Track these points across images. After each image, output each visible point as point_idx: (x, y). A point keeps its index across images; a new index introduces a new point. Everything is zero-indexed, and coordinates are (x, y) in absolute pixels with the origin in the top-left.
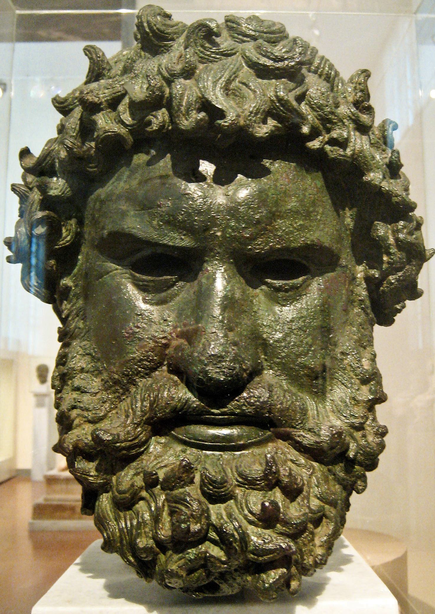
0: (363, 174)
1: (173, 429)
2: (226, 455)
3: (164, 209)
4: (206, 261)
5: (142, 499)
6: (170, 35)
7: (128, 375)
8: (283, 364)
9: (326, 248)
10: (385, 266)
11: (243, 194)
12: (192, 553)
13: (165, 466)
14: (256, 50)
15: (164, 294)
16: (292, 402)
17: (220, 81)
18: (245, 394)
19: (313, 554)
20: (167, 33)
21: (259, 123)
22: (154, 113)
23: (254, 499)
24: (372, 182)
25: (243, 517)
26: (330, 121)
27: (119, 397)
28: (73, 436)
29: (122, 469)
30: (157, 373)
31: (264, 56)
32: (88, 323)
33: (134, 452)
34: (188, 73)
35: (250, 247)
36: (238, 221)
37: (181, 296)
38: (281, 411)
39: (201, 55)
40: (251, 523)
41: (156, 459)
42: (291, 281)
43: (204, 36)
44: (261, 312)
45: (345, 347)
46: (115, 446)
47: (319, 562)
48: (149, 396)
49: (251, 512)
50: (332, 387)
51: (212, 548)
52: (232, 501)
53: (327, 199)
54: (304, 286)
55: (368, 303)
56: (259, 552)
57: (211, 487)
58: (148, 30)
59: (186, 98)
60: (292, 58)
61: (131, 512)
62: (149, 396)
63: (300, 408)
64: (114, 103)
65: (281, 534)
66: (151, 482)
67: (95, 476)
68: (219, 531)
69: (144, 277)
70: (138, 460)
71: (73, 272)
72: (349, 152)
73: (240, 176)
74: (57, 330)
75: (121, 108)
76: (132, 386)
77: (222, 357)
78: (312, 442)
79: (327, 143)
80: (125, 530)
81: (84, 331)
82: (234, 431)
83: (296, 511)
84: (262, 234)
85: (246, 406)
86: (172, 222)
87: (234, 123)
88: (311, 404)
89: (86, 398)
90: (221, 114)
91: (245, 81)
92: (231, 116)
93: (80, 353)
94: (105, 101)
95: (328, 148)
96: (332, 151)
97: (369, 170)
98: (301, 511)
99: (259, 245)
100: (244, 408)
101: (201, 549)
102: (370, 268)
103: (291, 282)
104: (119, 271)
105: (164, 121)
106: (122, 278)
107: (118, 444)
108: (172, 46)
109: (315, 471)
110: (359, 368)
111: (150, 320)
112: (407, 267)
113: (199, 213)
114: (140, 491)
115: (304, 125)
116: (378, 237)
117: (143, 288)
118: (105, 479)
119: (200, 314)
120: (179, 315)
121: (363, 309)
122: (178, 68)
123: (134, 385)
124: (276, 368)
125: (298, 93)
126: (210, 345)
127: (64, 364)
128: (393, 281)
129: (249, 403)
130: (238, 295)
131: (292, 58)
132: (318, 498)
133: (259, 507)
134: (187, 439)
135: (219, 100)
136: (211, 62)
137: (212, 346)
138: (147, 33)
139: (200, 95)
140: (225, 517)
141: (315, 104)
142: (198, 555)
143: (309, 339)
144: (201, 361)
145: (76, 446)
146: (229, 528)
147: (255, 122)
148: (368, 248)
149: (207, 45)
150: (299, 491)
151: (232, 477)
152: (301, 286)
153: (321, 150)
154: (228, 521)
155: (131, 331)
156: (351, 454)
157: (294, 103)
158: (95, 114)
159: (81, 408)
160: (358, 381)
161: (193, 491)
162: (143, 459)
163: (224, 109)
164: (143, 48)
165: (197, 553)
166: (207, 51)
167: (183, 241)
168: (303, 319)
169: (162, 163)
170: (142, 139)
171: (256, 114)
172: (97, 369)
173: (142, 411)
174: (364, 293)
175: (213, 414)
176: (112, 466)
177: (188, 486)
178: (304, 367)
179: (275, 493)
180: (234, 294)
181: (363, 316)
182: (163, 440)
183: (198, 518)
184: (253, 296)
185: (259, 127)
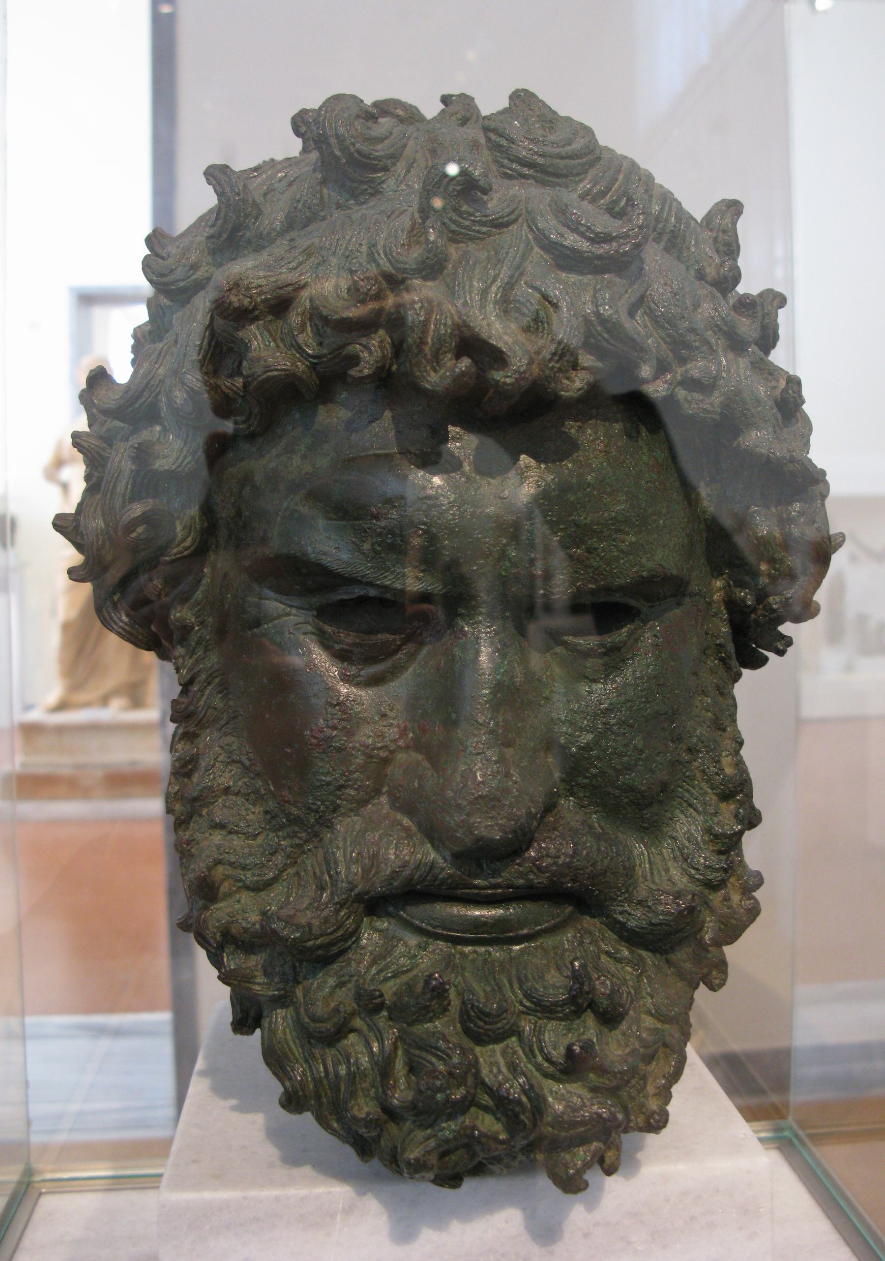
0: (736, 432)
4: (462, 616)
6: (380, 161)
12: (449, 1128)
13: (395, 975)
14: (556, 216)
17: (494, 288)
20: (375, 159)
21: (567, 371)
22: (364, 341)
25: (535, 1067)
26: (688, 346)
28: (220, 913)
32: (231, 703)
34: (432, 268)
39: (453, 227)
40: (546, 1075)
41: (374, 962)
43: (458, 191)
46: (305, 947)
49: (548, 1059)
50: (672, 813)
51: (480, 1117)
52: (514, 1039)
55: (731, 648)
57: (481, 1023)
58: (338, 153)
60: (626, 236)
61: (333, 1051)
63: (625, 868)
66: (370, 1004)
67: (264, 983)
70: (341, 959)
71: (195, 596)
72: (716, 399)
79: (681, 384)
80: (325, 1082)
82: (512, 910)
83: (620, 1045)
85: (534, 873)
92: (518, 362)
93: (221, 758)
94: (262, 301)
95: (681, 393)
97: (750, 425)
98: (627, 1045)
102: (736, 586)
105: (384, 357)
107: (311, 943)
110: (719, 775)
115: (644, 362)
119: (454, 716)
121: (722, 660)
122: (415, 254)
123: (328, 827)
127: (189, 775)
129: (540, 869)
132: (652, 1015)
133: (562, 1050)
135: (499, 330)
136: (472, 239)
138: (337, 159)
140: (504, 1070)
142: (458, 1132)
147: (560, 370)
149: (465, 208)
154: (511, 1076)
155: (322, 736)
159: (231, 864)
165: (458, 1128)
166: (464, 219)
169: (376, 427)
172: (256, 792)
177: (439, 1018)
179: (585, 1022)
180: (512, 677)
185: (568, 378)
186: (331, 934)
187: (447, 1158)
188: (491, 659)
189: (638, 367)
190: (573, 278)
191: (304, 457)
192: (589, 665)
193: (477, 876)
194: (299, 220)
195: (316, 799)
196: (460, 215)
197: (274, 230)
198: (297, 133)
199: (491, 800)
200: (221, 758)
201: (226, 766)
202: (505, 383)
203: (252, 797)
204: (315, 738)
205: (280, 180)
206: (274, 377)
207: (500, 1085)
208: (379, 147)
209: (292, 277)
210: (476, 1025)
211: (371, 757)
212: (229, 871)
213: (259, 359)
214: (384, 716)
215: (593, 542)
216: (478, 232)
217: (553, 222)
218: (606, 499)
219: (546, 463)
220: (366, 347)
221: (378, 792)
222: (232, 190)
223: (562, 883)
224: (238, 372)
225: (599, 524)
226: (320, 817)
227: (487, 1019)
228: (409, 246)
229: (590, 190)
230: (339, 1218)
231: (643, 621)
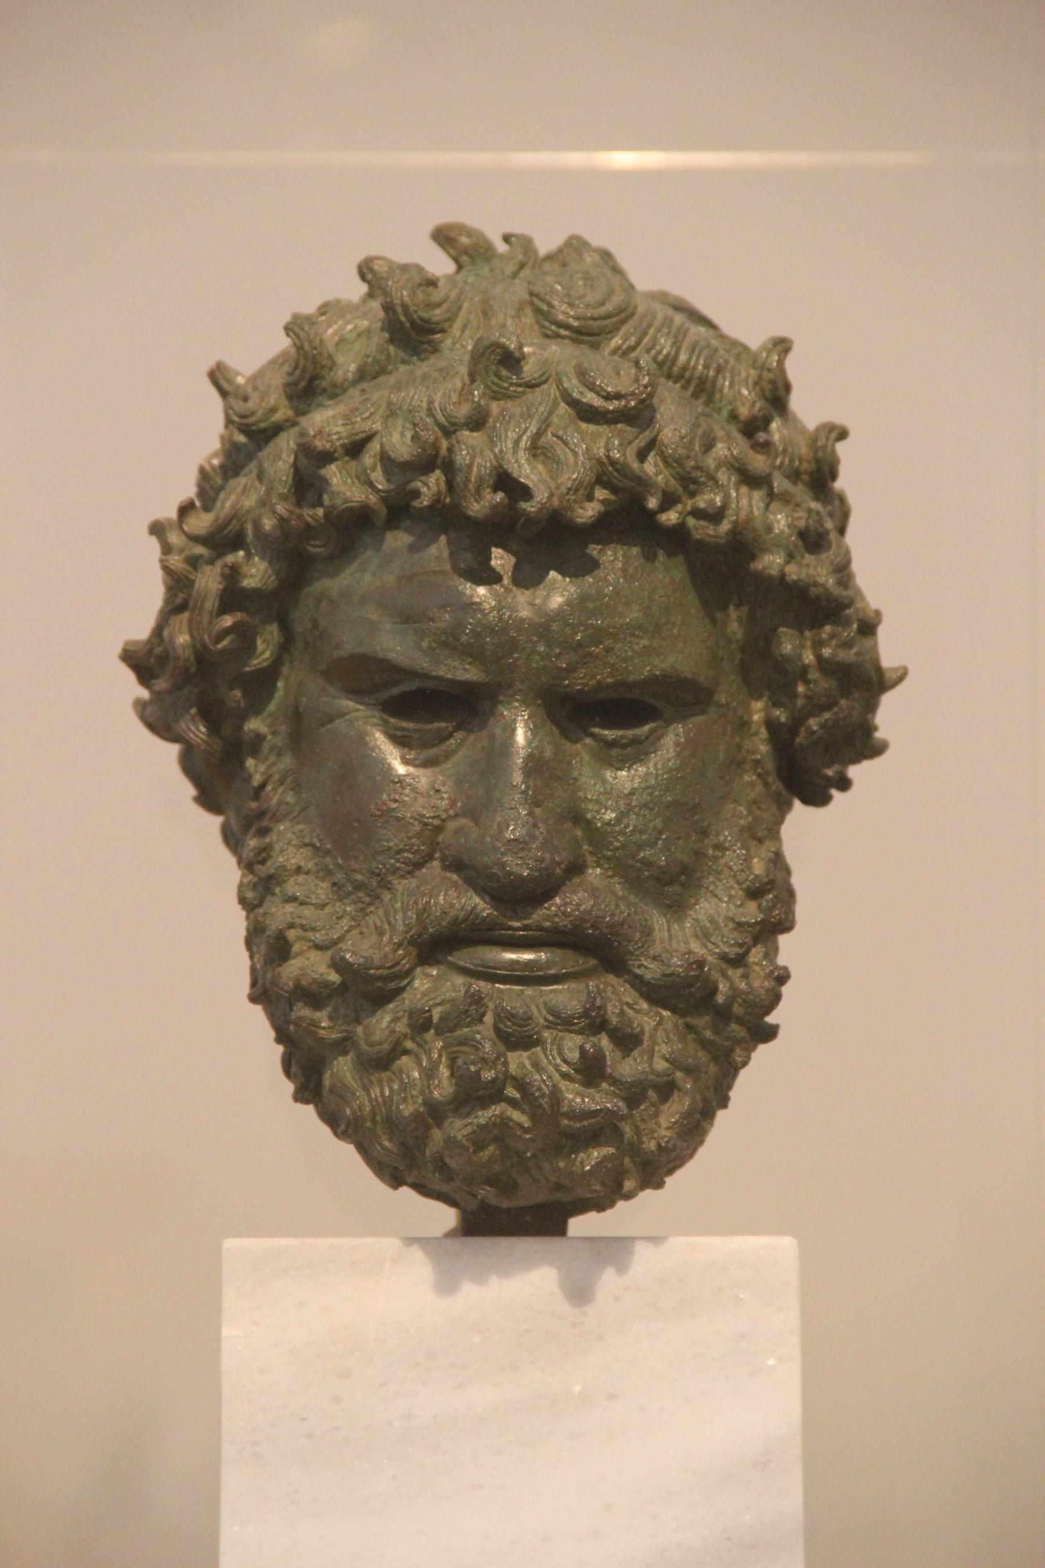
0: (752, 557)
1: (450, 953)
2: (529, 991)
3: (438, 625)
4: (501, 702)
5: (406, 1052)
7: (379, 875)
8: (618, 859)
9: (687, 680)
10: (800, 702)
11: (557, 601)
15: (434, 750)
16: (629, 915)
17: (525, 438)
18: (558, 900)
21: (581, 502)
22: (424, 478)
26: (695, 481)
27: (362, 910)
29: (373, 1012)
30: (424, 870)
31: (591, 390)
32: (304, 796)
33: (392, 985)
34: (478, 422)
36: (549, 645)
37: (460, 753)
38: (610, 926)
39: (495, 388)
40: (565, 1076)
44: (583, 780)
45: (722, 838)
47: (663, 1144)
48: (416, 903)
52: (539, 1049)
53: (692, 599)
54: (651, 738)
56: (574, 1115)
57: (509, 1024)
58: (403, 318)
61: (387, 1073)
62: (416, 903)
63: (641, 925)
64: (355, 449)
66: (421, 1024)
67: (329, 1028)
68: (521, 1085)
69: (404, 724)
71: (268, 709)
72: (725, 526)
73: (553, 574)
76: (386, 892)
77: (524, 842)
78: (658, 976)
80: (380, 1099)
81: (297, 809)
86: (450, 642)
88: (658, 921)
89: (307, 912)
90: (525, 492)
91: (560, 433)
92: (541, 495)
93: (294, 842)
95: (691, 522)
97: (765, 551)
100: (557, 919)
103: (630, 733)
104: (361, 714)
105: (439, 493)
106: (366, 723)
108: (441, 342)
111: (414, 790)
112: (843, 702)
113: (492, 630)
116: (781, 656)
117: (400, 740)
118: (346, 1031)
120: (459, 782)
121: (759, 775)
122: (463, 411)
123: (389, 889)
124: (606, 866)
126: (508, 826)
128: (815, 728)
129: (564, 913)
130: (548, 753)
132: (667, 1060)
134: (472, 967)
135: (527, 471)
136: (509, 397)
137: (511, 828)
138: (401, 323)
140: (529, 1067)
141: (671, 455)
143: (658, 823)
144: (496, 849)
145: (298, 986)
147: (575, 502)
148: (762, 668)
151: (540, 1017)
152: (647, 738)
153: (681, 529)
155: (385, 808)
156: (720, 999)
157: (635, 465)
158: (324, 466)
160: (741, 893)
161: (484, 1032)
162: (404, 999)
164: (391, 340)
167: (471, 673)
168: (650, 791)
169: (433, 550)
170: (399, 510)
171: (577, 490)
173: (406, 925)
174: (764, 748)
175: (511, 928)
178: (647, 863)
180: (541, 752)
181: (760, 788)
184: (570, 755)
185: (582, 508)
186: (389, 968)
188: (526, 738)
189: (645, 499)
190: (592, 428)
191: (374, 574)
193: (511, 919)
194: (370, 373)
195: (379, 863)
196: (500, 378)
197: (346, 380)
198: (363, 277)
199: (520, 843)
200: (294, 842)
201: (298, 850)
202: (531, 512)
203: (321, 874)
204: (379, 810)
205: (350, 331)
206: (351, 508)
208: (438, 311)
209: (367, 426)
210: (505, 1025)
212: (300, 932)
213: (338, 493)
214: (438, 791)
216: (515, 392)
217: (575, 382)
218: (620, 608)
219: (570, 577)
220: (426, 484)
221: (430, 857)
222: (311, 345)
223: (585, 929)
224: (319, 503)
225: (615, 628)
226: (383, 879)
228: (460, 403)
229: (621, 345)
231: (666, 722)
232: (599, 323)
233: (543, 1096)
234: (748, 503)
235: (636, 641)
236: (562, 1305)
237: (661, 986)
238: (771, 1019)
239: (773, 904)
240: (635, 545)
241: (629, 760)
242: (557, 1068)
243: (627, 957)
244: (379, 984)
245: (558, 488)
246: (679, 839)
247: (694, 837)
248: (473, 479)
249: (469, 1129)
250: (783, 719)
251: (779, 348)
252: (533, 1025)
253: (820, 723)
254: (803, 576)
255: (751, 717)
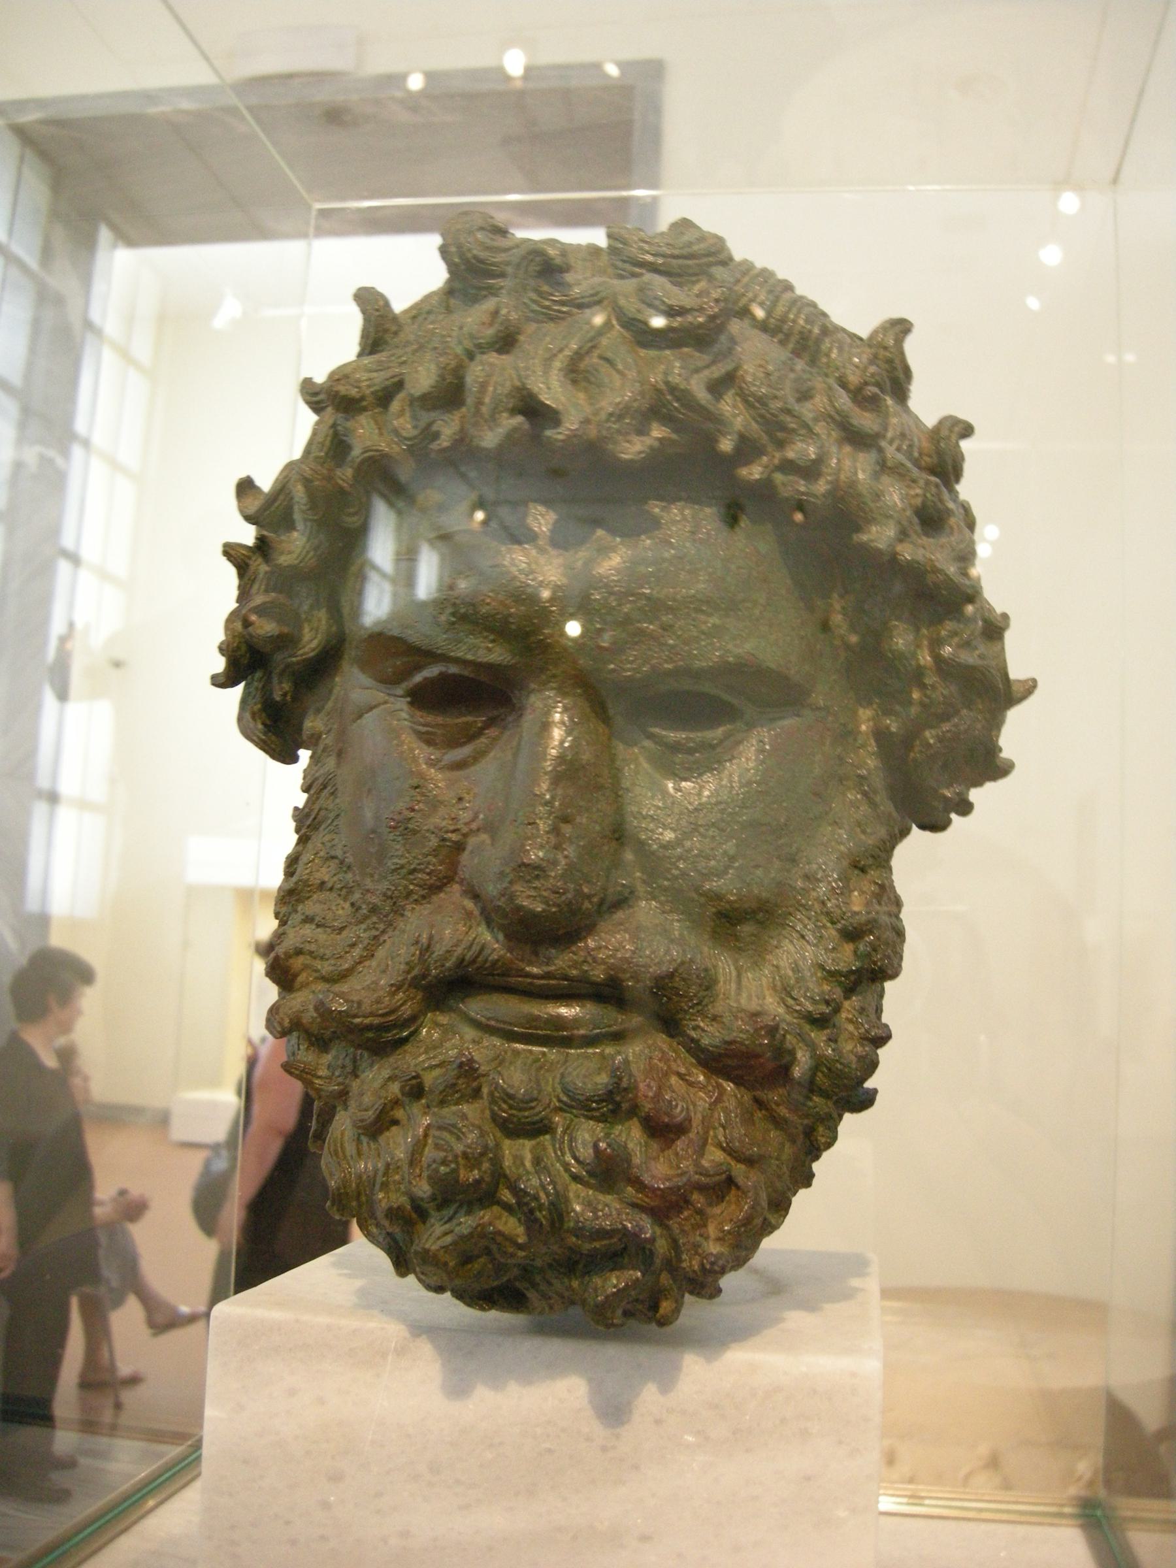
0: (858, 529)
17: (561, 356)
18: (591, 943)
19: (700, 1251)
20: (493, 264)
21: (627, 434)
23: (587, 1136)
24: (872, 545)
26: (783, 428)
30: (442, 895)
33: (388, 1036)
35: (612, 666)
40: (576, 1178)
42: (699, 734)
44: (637, 790)
45: (815, 866)
47: (708, 1267)
50: (779, 941)
51: (504, 1219)
52: (547, 1137)
57: (505, 1106)
59: (491, 389)
60: (701, 310)
65: (634, 1205)
72: (821, 487)
74: (290, 812)
75: (395, 406)
78: (717, 1042)
84: (636, 643)
87: (575, 436)
91: (609, 355)
92: (571, 424)
93: (322, 854)
94: (372, 393)
95: (779, 477)
96: (790, 486)
97: (871, 521)
99: (632, 662)
101: (483, 1218)
103: (698, 735)
109: (725, 1098)
114: (392, 1109)
118: (343, 1084)
125: (716, 375)
131: (701, 310)
132: (723, 1149)
134: (483, 1020)
135: (551, 390)
136: (552, 319)
139: (518, 384)
140: (528, 1164)
146: (531, 1183)
147: (619, 431)
148: (873, 670)
149: (546, 288)
150: (680, 1129)
152: (721, 741)
163: (561, 407)
167: (496, 654)
174: (871, 763)
176: (354, 1061)
181: (864, 808)
182: (443, 1019)
183: (476, 1159)
185: (628, 442)
186: (382, 1015)
187: (470, 1266)
189: (717, 441)
192: (678, 761)
193: (530, 963)
200: (322, 854)
202: (556, 440)
207: (519, 1178)
211: (444, 840)
215: (667, 618)
216: (559, 311)
219: (620, 536)
227: (511, 1102)
230: (390, 1358)
231: (747, 724)
232: (680, 261)
233: (541, 1207)
234: (857, 468)
235: (703, 617)
236: (596, 1428)
237: (720, 1055)
238: (869, 1084)
239: (871, 957)
240: (710, 506)
241: (698, 768)
242: (566, 1166)
243: (680, 1016)
244: (370, 1035)
245: (596, 414)
246: (757, 866)
247: (777, 864)
248: (487, 400)
249: (448, 1239)
250: (893, 729)
251: (898, 328)
252: (539, 1108)
253: (938, 736)
254: (920, 558)
255: (859, 727)
